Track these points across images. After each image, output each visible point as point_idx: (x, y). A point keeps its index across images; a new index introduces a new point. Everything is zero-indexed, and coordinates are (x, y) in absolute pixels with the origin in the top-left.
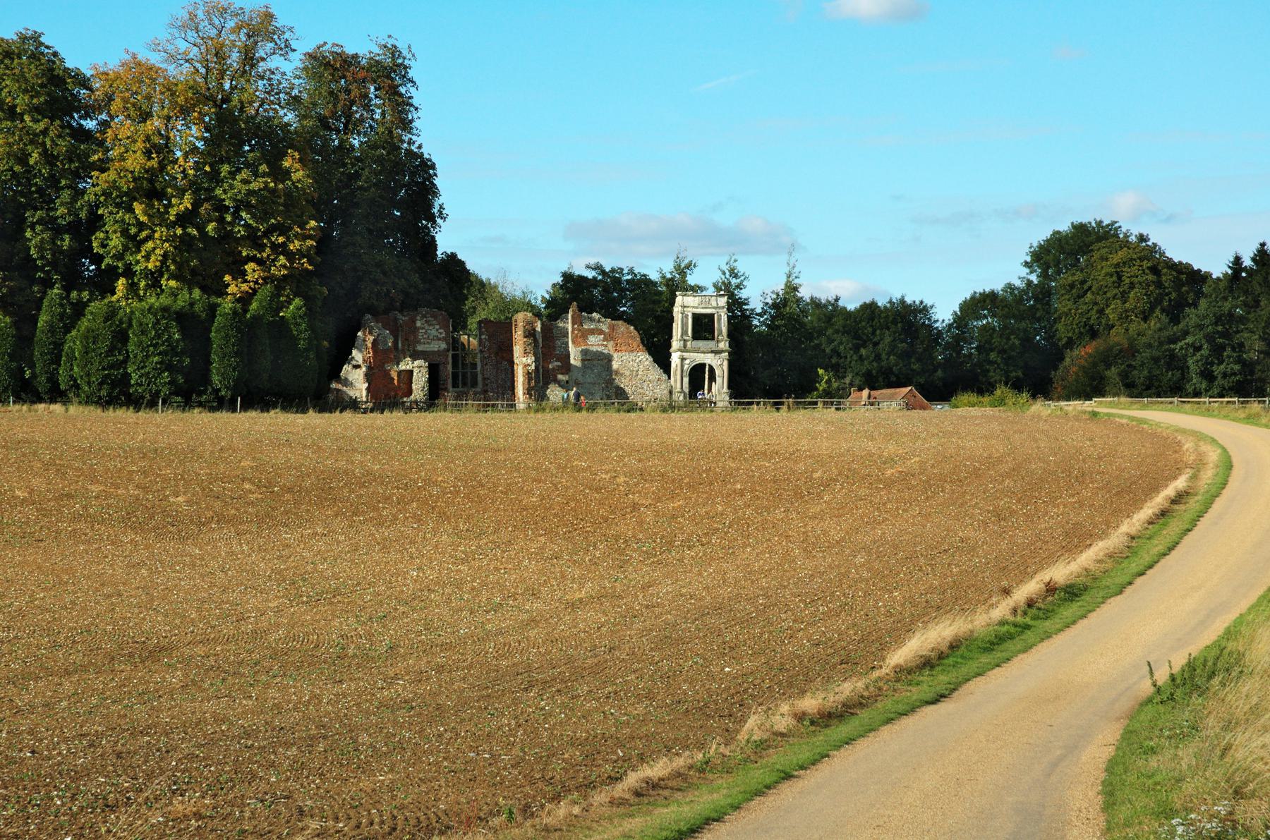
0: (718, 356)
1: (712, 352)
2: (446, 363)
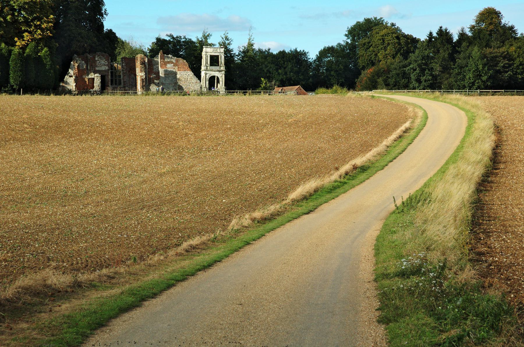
0: (220, 73)
1: (218, 71)
2: (108, 75)
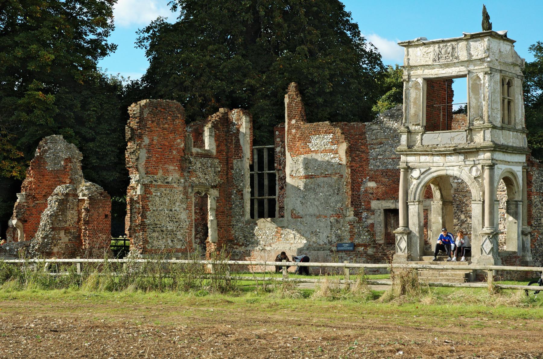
0: (470, 161)
1: (456, 151)
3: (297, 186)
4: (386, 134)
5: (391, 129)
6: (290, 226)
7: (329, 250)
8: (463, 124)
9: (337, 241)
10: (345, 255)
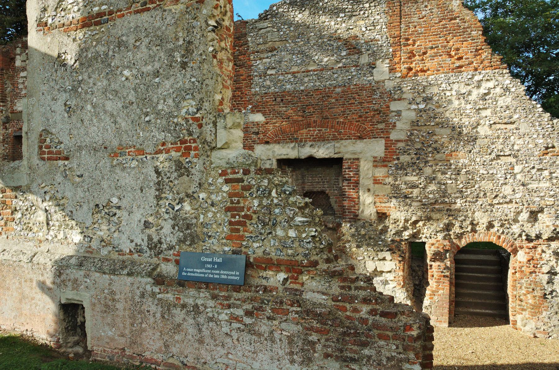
3: (55, 54)
4: (282, 33)
5: (290, 25)
6: (35, 185)
7: (150, 275)
8: (426, 6)
9: (181, 241)
10: (211, 303)
